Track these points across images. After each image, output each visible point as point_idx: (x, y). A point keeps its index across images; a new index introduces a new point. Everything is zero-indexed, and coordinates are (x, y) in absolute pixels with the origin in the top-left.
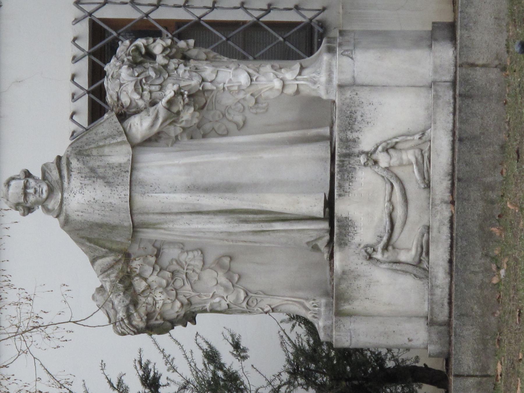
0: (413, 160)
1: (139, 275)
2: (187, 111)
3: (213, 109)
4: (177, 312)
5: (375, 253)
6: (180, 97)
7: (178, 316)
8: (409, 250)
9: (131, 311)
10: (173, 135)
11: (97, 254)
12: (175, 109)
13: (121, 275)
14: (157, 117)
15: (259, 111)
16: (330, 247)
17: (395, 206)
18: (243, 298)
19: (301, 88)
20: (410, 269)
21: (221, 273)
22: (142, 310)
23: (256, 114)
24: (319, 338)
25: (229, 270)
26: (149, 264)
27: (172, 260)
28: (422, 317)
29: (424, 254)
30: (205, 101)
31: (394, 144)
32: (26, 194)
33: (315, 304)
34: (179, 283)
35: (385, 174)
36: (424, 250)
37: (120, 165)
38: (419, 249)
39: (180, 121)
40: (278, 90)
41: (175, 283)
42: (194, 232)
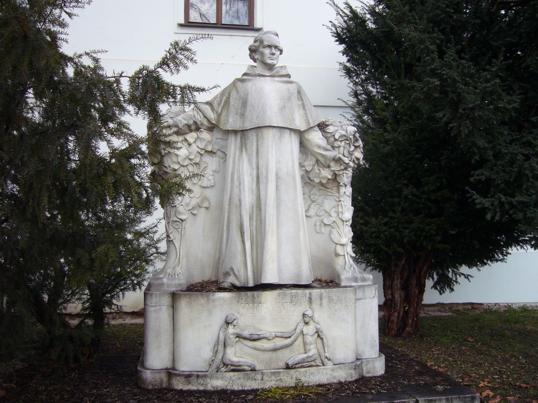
0: (310, 354)
1: (198, 138)
2: (329, 174)
3: (319, 193)
4: (170, 167)
5: (233, 326)
7: (166, 167)
8: (235, 355)
9: (173, 129)
10: (306, 164)
11: (215, 105)
12: (332, 164)
13: (199, 123)
14: (327, 150)
15: (318, 227)
16: (230, 287)
17: (272, 341)
18: (181, 217)
19: (341, 258)
20: (220, 356)
21: (198, 200)
23: (315, 225)
24: (341, 385)
25: (200, 207)
26: (206, 145)
27: (207, 163)
28: (174, 360)
29: (232, 368)
30: (329, 187)
31: (321, 337)
32: (270, 46)
33: (179, 274)
34: (191, 168)
35: (298, 331)
36: (237, 368)
37: (294, 120)
38: (238, 364)
39: (320, 168)
40: (340, 241)
41: (191, 165)
42: (239, 178)
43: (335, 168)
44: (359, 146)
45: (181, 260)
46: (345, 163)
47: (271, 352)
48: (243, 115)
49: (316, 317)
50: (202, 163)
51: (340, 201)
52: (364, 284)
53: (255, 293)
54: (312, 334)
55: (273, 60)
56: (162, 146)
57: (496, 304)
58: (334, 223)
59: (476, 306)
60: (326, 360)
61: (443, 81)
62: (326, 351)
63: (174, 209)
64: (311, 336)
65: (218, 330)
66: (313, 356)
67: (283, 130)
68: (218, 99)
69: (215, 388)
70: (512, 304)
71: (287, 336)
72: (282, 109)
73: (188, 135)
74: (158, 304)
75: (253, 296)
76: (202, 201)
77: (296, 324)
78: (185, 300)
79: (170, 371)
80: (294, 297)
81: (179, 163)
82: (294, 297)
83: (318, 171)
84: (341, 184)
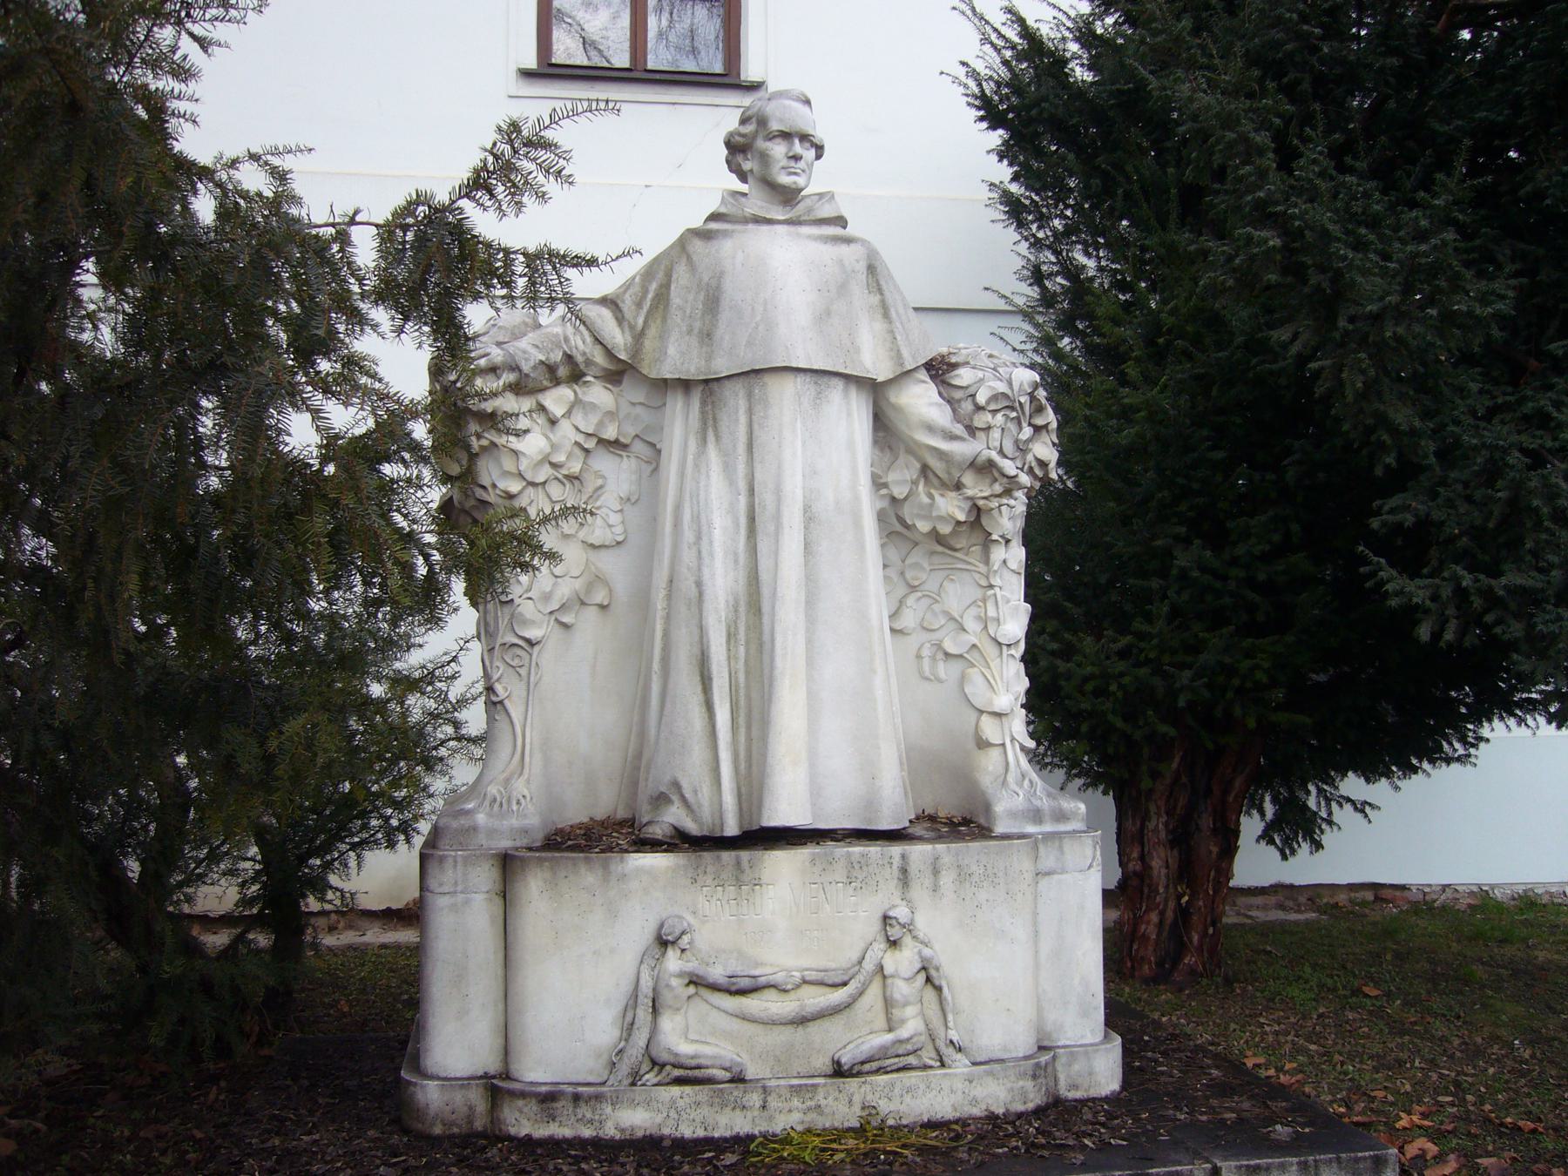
0: (904, 1033)
1: (577, 403)
2: (959, 507)
3: (930, 564)
4: (494, 486)
5: (679, 952)
6: (998, 488)
7: (484, 487)
9: (504, 376)
10: (891, 477)
11: (627, 305)
12: (968, 479)
13: (580, 359)
14: (953, 437)
16: (672, 837)
17: (792, 995)
20: (640, 1039)
21: (578, 585)
22: (508, 403)
23: (919, 657)
25: (583, 603)
26: (601, 424)
27: (603, 477)
28: (506, 1052)
29: (677, 1073)
30: (958, 546)
31: (937, 982)
32: (786, 136)
34: (555, 491)
35: (869, 965)
36: (690, 1073)
37: (858, 351)
38: (693, 1062)
39: (932, 491)
40: (991, 703)
41: (556, 482)
42: (696, 519)
43: (976, 491)
44: (1046, 427)
45: (527, 759)
46: (1004, 475)
47: (790, 1029)
48: (707, 336)
49: (922, 924)
50: (587, 477)
51: (991, 586)
52: (1062, 828)
53: (745, 855)
54: (908, 974)
55: (795, 174)
56: (473, 427)
57: (1445, 887)
58: (975, 650)
59: (1386, 894)
60: (951, 1050)
61: (1291, 235)
62: (951, 1024)
63: (507, 609)
64: (907, 980)
65: (636, 963)
66: (911, 1038)
67: (825, 379)
68: (636, 289)
69: (628, 1133)
70: (1493, 887)
71: (838, 980)
72: (823, 317)
73: (548, 393)
74: (459, 888)
75: (738, 863)
76: (590, 587)
77: (862, 945)
78: (539, 874)
79: (495, 1081)
80: (857, 866)
81: (521, 475)
82: (857, 866)
83: (926, 500)
84: (995, 537)
